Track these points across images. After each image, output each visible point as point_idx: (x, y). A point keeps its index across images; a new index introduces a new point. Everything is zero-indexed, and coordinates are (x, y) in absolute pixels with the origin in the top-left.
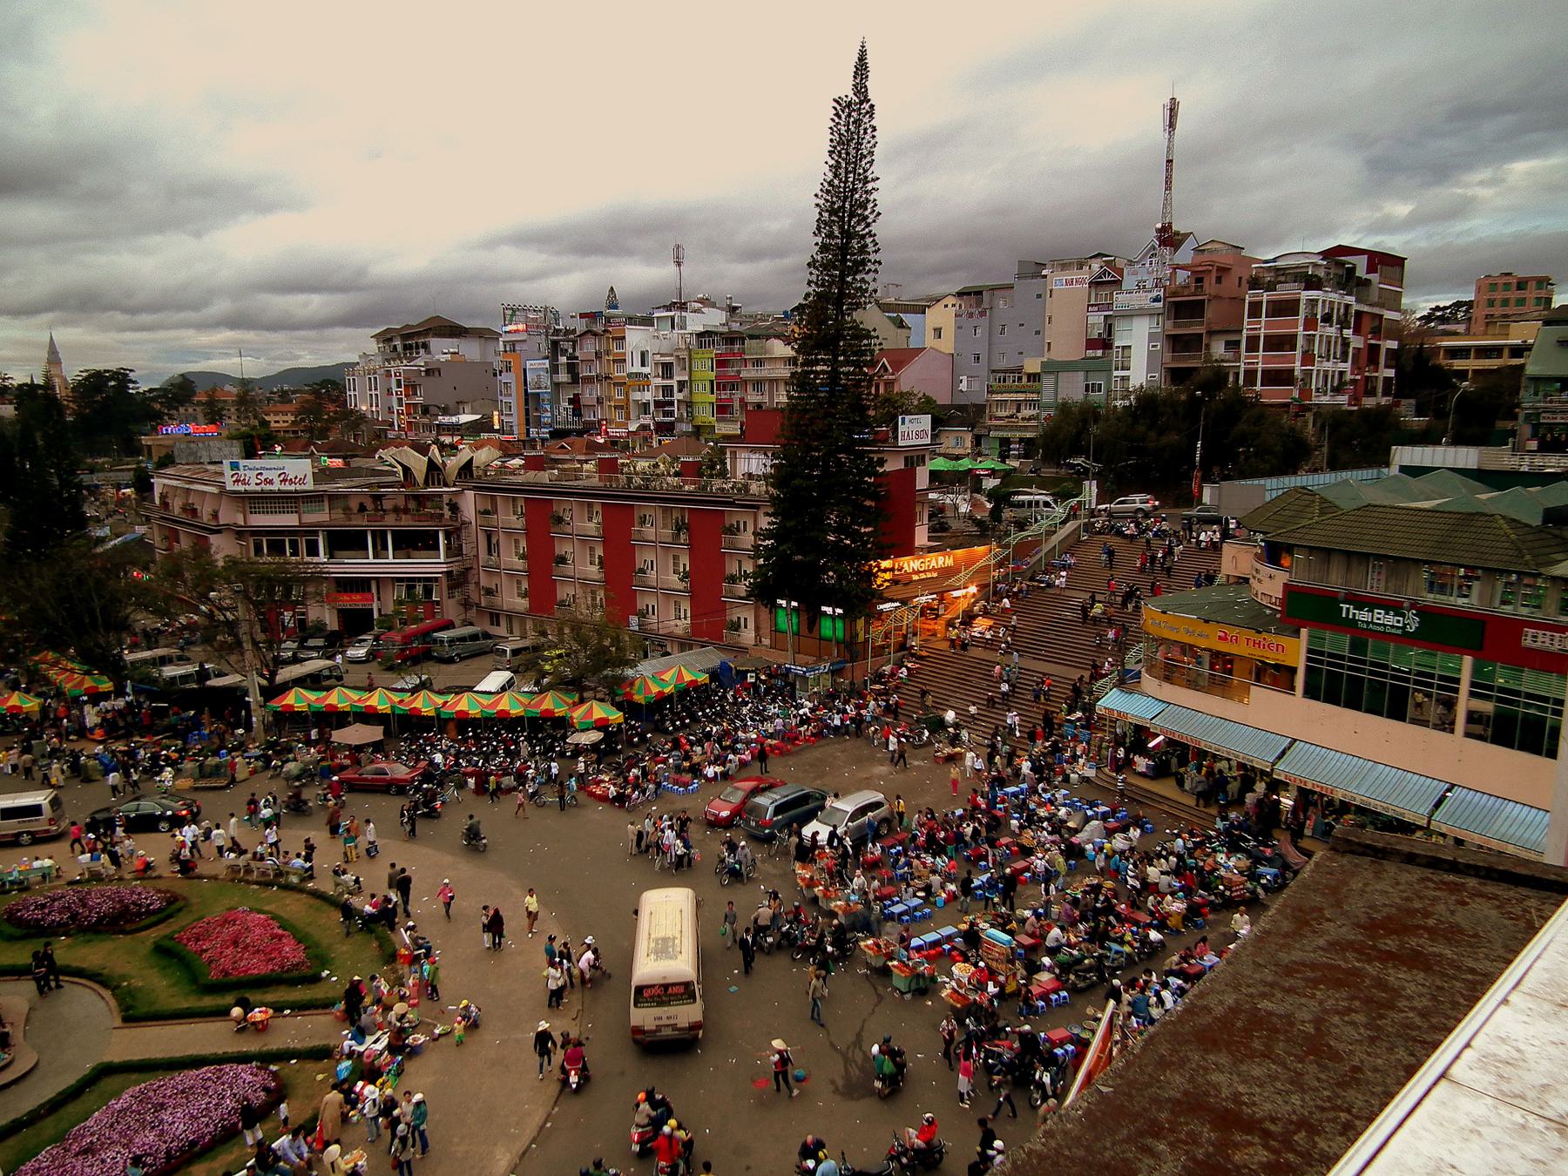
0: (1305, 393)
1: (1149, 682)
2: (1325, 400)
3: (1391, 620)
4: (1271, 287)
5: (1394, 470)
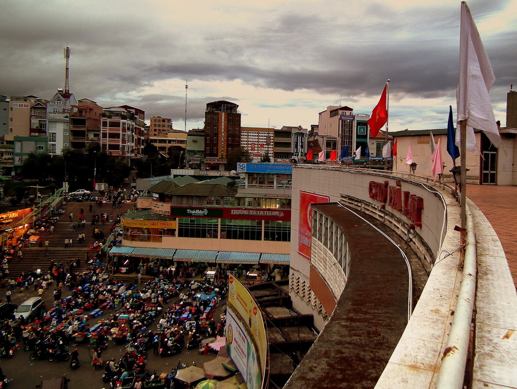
0: (124, 153)
1: (125, 242)
2: (129, 155)
3: (201, 212)
4: (110, 117)
5: (172, 176)
